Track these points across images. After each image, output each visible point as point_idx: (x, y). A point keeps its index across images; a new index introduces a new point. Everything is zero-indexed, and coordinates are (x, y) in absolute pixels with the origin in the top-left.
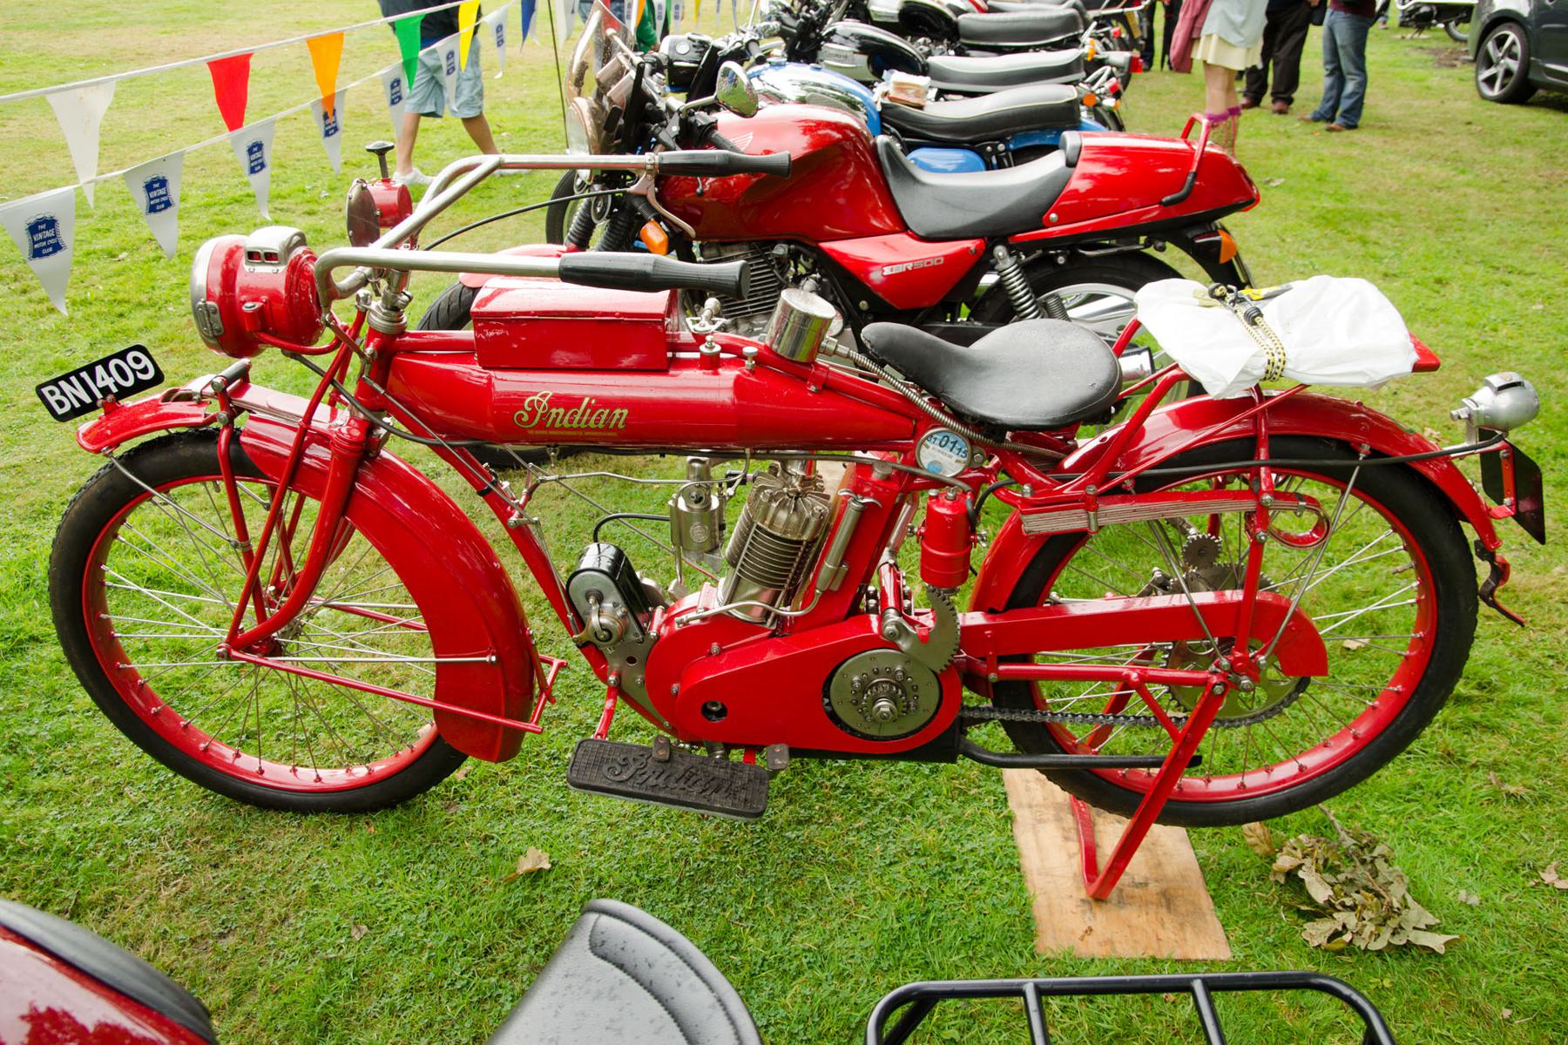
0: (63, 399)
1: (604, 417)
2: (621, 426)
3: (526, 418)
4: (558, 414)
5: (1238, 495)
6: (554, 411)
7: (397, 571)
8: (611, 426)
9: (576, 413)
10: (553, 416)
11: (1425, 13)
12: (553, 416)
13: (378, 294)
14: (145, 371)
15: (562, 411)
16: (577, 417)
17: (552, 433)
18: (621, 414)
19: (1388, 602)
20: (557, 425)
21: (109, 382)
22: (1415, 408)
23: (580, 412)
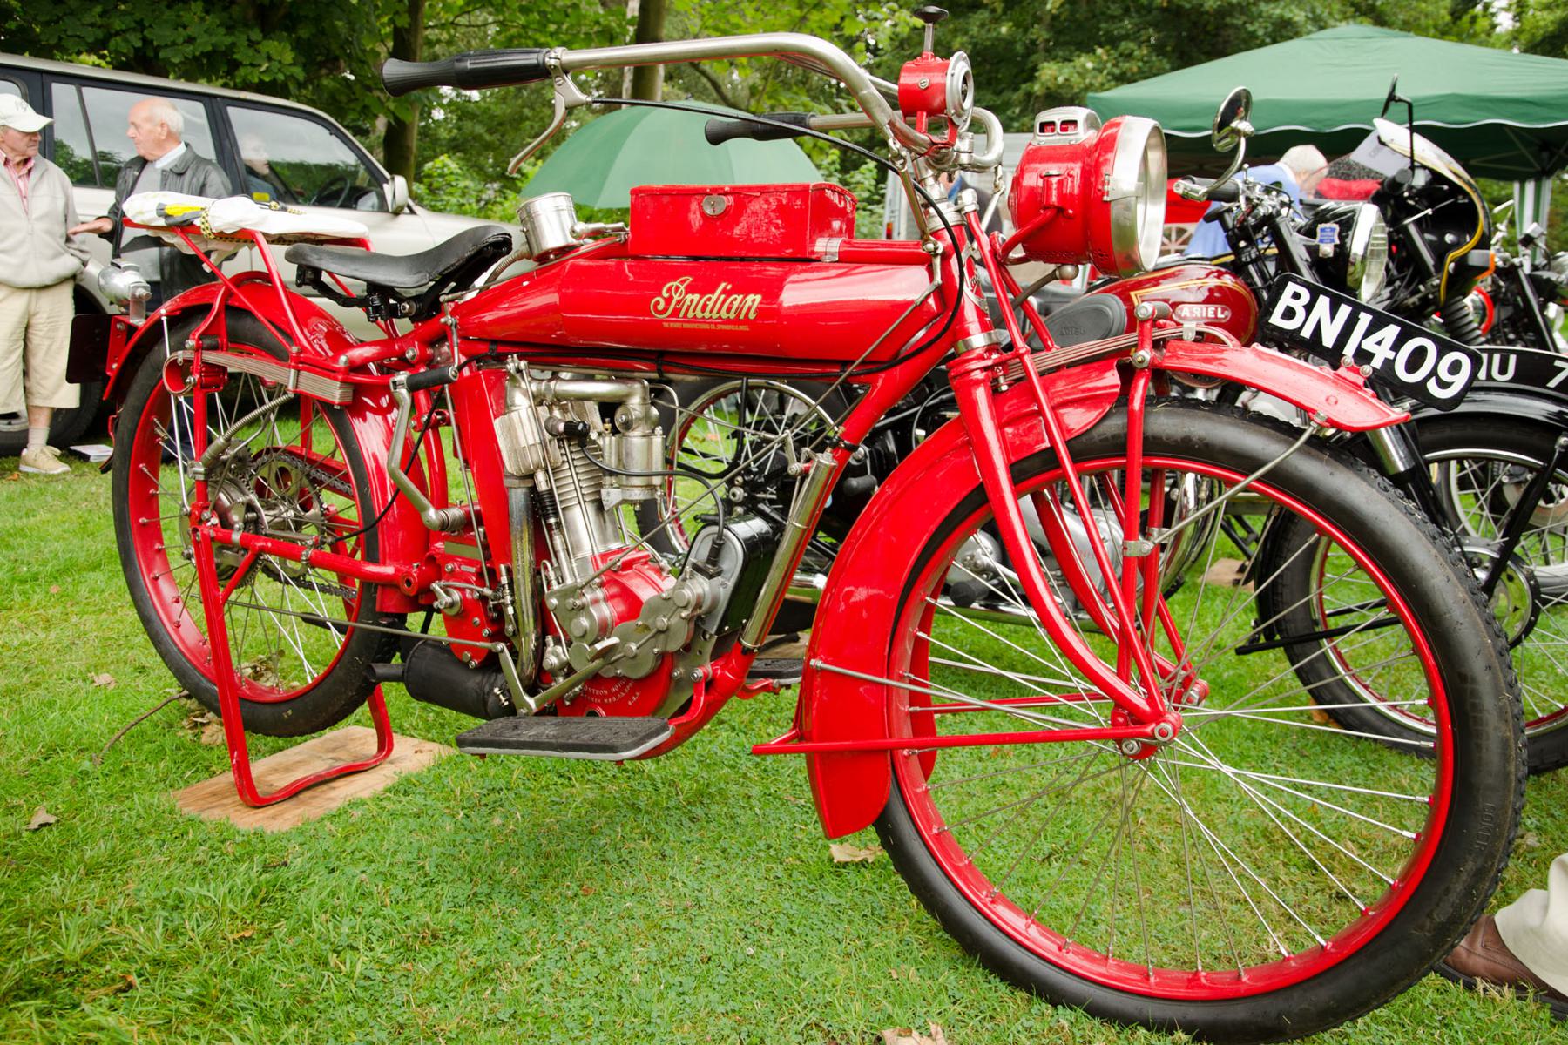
0: (1301, 313)
1: (736, 304)
2: (752, 316)
3: (660, 307)
4: (692, 301)
5: (124, 13)
6: (689, 297)
7: (250, 773)
8: (742, 317)
9: (709, 299)
10: (688, 303)
11: (829, 534)
12: (688, 303)
13: (456, 17)
14: (1443, 385)
15: (696, 297)
16: (710, 304)
17: (686, 326)
18: (754, 301)
19: (961, 659)
20: (690, 315)
21: (1381, 354)
22: (675, 645)
23: (714, 298)
